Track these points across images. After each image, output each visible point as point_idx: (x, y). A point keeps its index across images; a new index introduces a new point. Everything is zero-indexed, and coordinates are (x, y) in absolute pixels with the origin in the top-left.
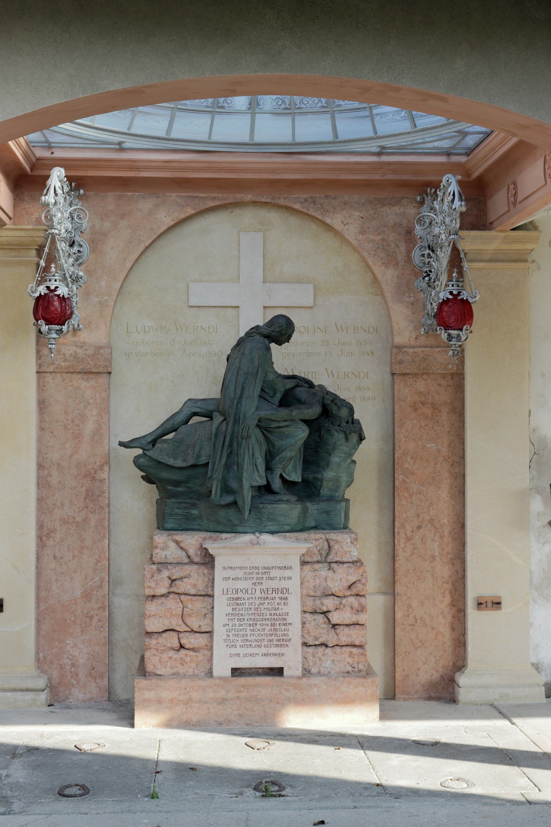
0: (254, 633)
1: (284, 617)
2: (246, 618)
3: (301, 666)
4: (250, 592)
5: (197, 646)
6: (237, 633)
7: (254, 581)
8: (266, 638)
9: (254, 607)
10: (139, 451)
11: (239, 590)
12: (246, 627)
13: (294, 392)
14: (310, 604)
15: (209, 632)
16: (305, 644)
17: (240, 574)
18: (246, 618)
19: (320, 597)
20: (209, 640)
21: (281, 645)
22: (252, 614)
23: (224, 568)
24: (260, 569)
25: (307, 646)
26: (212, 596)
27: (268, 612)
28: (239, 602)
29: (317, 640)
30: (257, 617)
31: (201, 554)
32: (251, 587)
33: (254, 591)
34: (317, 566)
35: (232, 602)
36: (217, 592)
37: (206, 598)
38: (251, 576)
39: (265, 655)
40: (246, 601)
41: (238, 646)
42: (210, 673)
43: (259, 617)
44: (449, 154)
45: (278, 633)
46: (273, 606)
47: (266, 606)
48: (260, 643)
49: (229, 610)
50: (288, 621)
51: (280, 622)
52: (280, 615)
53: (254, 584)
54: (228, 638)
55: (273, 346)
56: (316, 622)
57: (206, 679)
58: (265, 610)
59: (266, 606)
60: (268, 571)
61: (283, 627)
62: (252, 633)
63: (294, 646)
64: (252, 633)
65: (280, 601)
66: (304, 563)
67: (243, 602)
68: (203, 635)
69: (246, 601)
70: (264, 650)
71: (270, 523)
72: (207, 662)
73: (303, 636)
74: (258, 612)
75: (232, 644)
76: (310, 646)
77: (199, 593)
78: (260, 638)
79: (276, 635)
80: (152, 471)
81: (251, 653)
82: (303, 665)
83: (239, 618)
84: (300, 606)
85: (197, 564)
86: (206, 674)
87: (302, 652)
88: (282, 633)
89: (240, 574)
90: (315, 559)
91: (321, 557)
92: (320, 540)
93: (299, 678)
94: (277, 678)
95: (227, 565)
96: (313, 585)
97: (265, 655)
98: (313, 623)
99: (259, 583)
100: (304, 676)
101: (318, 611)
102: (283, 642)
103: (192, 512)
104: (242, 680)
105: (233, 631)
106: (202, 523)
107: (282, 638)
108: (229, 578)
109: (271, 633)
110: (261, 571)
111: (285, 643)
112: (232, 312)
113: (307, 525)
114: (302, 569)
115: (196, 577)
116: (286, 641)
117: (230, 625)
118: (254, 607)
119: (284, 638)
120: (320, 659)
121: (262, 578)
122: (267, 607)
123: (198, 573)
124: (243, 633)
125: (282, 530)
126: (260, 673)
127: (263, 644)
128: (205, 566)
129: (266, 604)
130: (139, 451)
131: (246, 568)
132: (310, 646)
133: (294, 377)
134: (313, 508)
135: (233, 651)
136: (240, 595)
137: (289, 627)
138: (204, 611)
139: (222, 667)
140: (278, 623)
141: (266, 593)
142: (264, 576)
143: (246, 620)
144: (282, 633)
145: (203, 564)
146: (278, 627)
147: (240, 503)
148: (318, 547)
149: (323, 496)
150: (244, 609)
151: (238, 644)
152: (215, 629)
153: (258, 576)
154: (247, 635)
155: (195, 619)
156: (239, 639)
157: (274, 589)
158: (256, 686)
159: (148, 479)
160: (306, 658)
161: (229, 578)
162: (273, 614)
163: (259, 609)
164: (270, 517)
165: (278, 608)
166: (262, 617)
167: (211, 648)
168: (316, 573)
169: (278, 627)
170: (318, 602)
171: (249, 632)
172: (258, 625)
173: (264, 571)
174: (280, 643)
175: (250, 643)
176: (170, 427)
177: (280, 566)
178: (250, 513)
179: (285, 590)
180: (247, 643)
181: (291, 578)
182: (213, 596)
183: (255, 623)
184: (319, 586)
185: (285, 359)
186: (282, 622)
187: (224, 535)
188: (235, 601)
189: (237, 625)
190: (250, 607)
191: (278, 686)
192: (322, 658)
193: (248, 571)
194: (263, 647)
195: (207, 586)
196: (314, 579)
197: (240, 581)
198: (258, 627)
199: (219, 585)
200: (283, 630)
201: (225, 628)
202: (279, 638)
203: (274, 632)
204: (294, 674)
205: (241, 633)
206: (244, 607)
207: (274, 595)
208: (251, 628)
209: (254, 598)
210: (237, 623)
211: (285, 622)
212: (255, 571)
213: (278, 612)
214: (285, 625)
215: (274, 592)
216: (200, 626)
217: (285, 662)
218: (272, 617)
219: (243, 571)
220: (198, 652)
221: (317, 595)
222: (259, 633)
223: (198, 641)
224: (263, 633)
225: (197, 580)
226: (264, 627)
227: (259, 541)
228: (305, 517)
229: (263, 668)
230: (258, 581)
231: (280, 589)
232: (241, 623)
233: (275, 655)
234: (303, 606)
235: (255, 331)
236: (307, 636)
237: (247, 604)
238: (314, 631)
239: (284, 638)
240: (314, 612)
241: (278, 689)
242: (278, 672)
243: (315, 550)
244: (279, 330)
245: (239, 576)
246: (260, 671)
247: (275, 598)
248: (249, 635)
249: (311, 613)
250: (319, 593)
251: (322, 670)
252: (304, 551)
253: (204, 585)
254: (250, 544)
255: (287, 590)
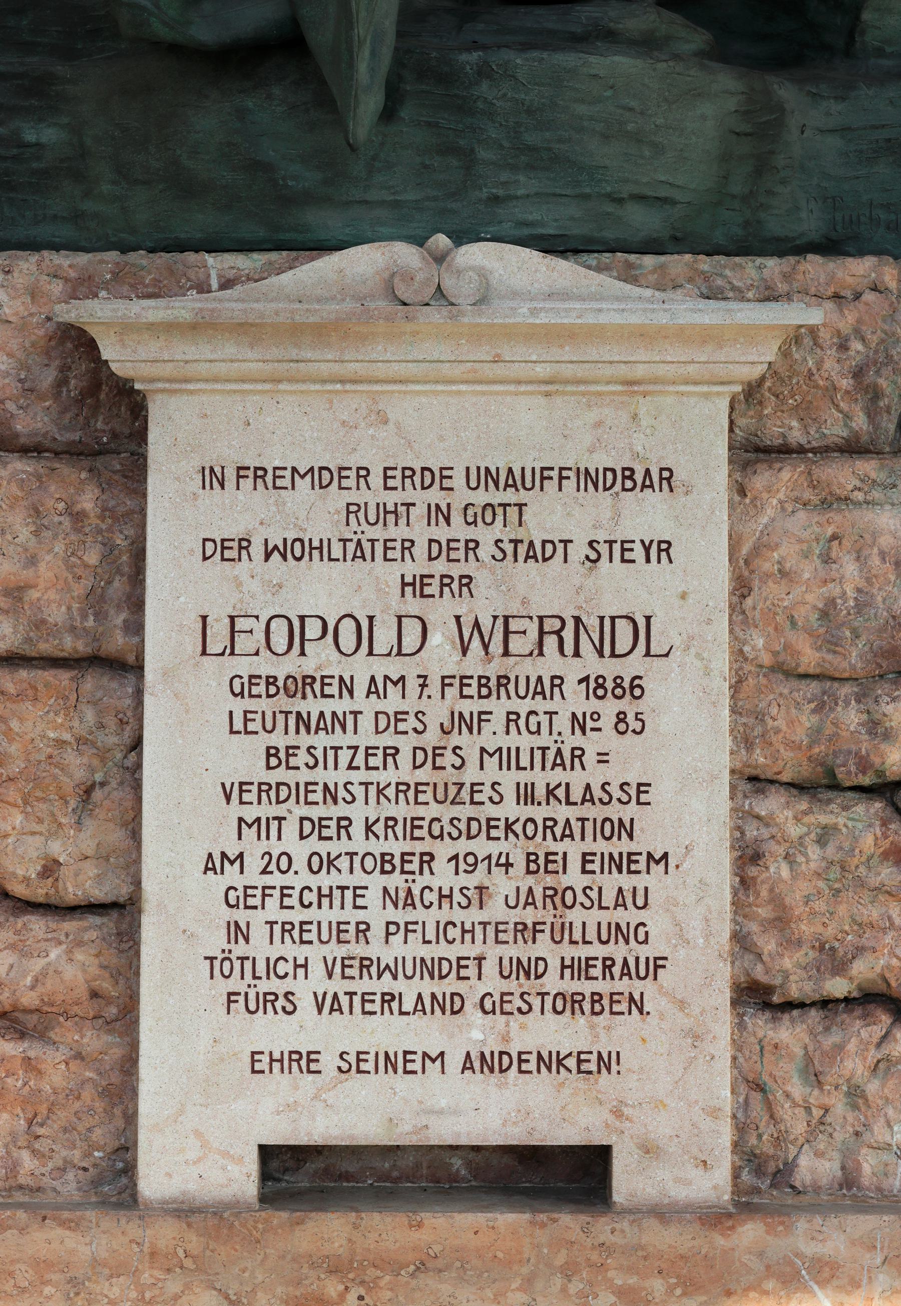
0: (411, 915)
1: (615, 811)
2: (358, 813)
3: (726, 1135)
4: (384, 638)
5: (29, 999)
6: (297, 916)
7: (411, 569)
8: (493, 952)
9: (413, 740)
11: (313, 629)
12: (359, 879)
14: (794, 722)
15: (115, 905)
16: (755, 996)
17: (317, 514)
18: (358, 813)
19: (865, 686)
20: (112, 958)
21: (596, 997)
22: (402, 788)
23: (212, 477)
24: (458, 481)
25: (767, 1005)
26: (128, 667)
27: (509, 780)
28: (312, 706)
29: (840, 967)
30: (434, 810)
31: (61, 383)
32: (396, 605)
33: (412, 631)
34: (844, 475)
35: (264, 705)
36: (164, 639)
37: (92, 682)
38: (393, 532)
39: (488, 1063)
40: (360, 701)
41: (305, 1003)
42: (115, 1179)
43: (446, 812)
45: (576, 916)
46: (544, 739)
47: (493, 735)
48: (450, 985)
49: (245, 760)
50: (646, 841)
51: (589, 845)
52: (588, 796)
53: (417, 586)
54: (240, 949)
56: (830, 850)
57: (91, 1214)
58: (491, 763)
59: (493, 735)
60: (510, 496)
61: (611, 882)
62: (401, 916)
63: (682, 1005)
64: (401, 916)
65: (595, 704)
66: (753, 453)
67: (341, 706)
68: (70, 925)
69: (360, 701)
70: (477, 1032)
71: (526, 184)
72: (99, 1105)
73: (741, 941)
74: (438, 778)
75: (264, 986)
76: (789, 1006)
77: (45, 647)
78: (452, 952)
79: (561, 933)
81: (395, 1047)
82: (741, 1129)
83: (315, 813)
84: (728, 743)
85: (31, 449)
86: (96, 1183)
87: (737, 1045)
88: (605, 917)
89: (317, 514)
90: (835, 429)
91: (872, 415)
92: (869, 297)
93: (714, 1218)
94: (569, 1222)
95: (229, 452)
96: (815, 598)
97: (488, 1063)
98: (814, 852)
99: (445, 581)
100: (744, 1205)
101: (849, 774)
102: (611, 981)
103: (30, 136)
104: (331, 1230)
105: (272, 903)
106: (88, 206)
107: (600, 951)
108: (244, 544)
109: (529, 916)
110: (461, 496)
111: (623, 985)
113: (774, 226)
114: (742, 491)
115: (24, 534)
116: (626, 971)
117: (254, 863)
118: (413, 740)
119: (618, 951)
120: (855, 1095)
121: (472, 546)
122: (504, 741)
123: (36, 512)
124: (335, 915)
125: (609, 234)
126: (454, 1178)
127: (473, 990)
128: (86, 462)
129: (498, 721)
131: (363, 473)
132: (789, 1006)
134: (813, 119)
135: (275, 1033)
136: (320, 658)
137: (652, 880)
138: (77, 766)
139: (198, 1132)
140: (574, 850)
141: (496, 647)
142: (486, 536)
143: (358, 829)
144: (605, 917)
145: (73, 452)
146: (574, 877)
147: (320, 37)
148: (857, 345)
149: (880, 52)
150: (345, 757)
151: (304, 990)
152: (149, 886)
153: (442, 533)
154: (363, 929)
155: (18, 819)
156: (314, 954)
157: (551, 625)
158: (421, 1267)
160: (760, 1088)
161: (244, 544)
162: (540, 792)
163: (449, 759)
164: (530, 138)
165: (578, 754)
166: (465, 811)
167: (119, 1010)
168: (837, 520)
169: (574, 877)
170: (852, 717)
171: (377, 914)
172: (441, 865)
173: (481, 497)
174: (587, 987)
175: (387, 983)
177: (598, 461)
178: (388, 114)
179: (624, 630)
180: (362, 987)
181: (665, 547)
182: (138, 668)
183: (419, 847)
184: (860, 607)
186: (601, 846)
187: (216, 264)
188: (283, 702)
189: (300, 863)
190: (388, 739)
191: (569, 1271)
192: (872, 1087)
193: (373, 496)
194: (472, 1012)
195: (95, 601)
196: (827, 559)
197: (318, 567)
198: (443, 876)
199: (177, 592)
200: (609, 899)
201: (218, 883)
202: (583, 952)
203: (547, 916)
204: (681, 1193)
205: (328, 915)
206: (349, 739)
207: (552, 663)
208: (396, 880)
209: (413, 684)
210: (300, 851)
211: (623, 846)
212: (423, 498)
213: (577, 779)
214: (623, 863)
215: (551, 642)
216: (50, 868)
217: (618, 1113)
218: (539, 813)
219: (337, 499)
220: (41, 1034)
221: (840, 665)
222: (445, 915)
223: (37, 965)
224: (474, 915)
225: (32, 561)
226: (479, 877)
227: (448, 283)
228: (762, 167)
229: (477, 1149)
230: (440, 567)
231: (592, 622)
232: (323, 848)
233: (553, 1062)
234: (749, 743)
236: (768, 944)
237: (366, 722)
238: (820, 905)
239: (618, 951)
240: (820, 785)
241: (575, 1287)
242: (574, 1176)
243: (830, 364)
245: (315, 533)
246: (457, 1163)
247: (558, 681)
248: (377, 931)
249: (799, 787)
250: (854, 657)
251: (869, 1164)
252: (754, 360)
253: (79, 589)
254: (382, 304)
255: (642, 630)
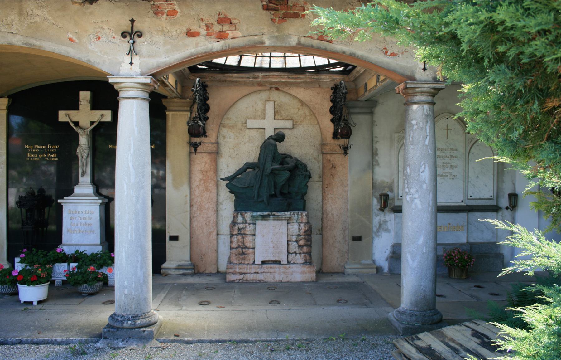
10: (228, 182)
13: (284, 158)
44: (194, 103)
55: (277, 143)
80: (232, 189)
112: (263, 130)
130: (228, 182)
133: (285, 154)
159: (231, 192)
176: (242, 171)
185: (282, 148)
235: (271, 137)
244: (280, 137)
